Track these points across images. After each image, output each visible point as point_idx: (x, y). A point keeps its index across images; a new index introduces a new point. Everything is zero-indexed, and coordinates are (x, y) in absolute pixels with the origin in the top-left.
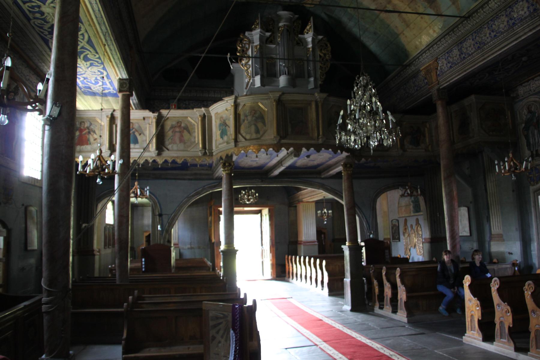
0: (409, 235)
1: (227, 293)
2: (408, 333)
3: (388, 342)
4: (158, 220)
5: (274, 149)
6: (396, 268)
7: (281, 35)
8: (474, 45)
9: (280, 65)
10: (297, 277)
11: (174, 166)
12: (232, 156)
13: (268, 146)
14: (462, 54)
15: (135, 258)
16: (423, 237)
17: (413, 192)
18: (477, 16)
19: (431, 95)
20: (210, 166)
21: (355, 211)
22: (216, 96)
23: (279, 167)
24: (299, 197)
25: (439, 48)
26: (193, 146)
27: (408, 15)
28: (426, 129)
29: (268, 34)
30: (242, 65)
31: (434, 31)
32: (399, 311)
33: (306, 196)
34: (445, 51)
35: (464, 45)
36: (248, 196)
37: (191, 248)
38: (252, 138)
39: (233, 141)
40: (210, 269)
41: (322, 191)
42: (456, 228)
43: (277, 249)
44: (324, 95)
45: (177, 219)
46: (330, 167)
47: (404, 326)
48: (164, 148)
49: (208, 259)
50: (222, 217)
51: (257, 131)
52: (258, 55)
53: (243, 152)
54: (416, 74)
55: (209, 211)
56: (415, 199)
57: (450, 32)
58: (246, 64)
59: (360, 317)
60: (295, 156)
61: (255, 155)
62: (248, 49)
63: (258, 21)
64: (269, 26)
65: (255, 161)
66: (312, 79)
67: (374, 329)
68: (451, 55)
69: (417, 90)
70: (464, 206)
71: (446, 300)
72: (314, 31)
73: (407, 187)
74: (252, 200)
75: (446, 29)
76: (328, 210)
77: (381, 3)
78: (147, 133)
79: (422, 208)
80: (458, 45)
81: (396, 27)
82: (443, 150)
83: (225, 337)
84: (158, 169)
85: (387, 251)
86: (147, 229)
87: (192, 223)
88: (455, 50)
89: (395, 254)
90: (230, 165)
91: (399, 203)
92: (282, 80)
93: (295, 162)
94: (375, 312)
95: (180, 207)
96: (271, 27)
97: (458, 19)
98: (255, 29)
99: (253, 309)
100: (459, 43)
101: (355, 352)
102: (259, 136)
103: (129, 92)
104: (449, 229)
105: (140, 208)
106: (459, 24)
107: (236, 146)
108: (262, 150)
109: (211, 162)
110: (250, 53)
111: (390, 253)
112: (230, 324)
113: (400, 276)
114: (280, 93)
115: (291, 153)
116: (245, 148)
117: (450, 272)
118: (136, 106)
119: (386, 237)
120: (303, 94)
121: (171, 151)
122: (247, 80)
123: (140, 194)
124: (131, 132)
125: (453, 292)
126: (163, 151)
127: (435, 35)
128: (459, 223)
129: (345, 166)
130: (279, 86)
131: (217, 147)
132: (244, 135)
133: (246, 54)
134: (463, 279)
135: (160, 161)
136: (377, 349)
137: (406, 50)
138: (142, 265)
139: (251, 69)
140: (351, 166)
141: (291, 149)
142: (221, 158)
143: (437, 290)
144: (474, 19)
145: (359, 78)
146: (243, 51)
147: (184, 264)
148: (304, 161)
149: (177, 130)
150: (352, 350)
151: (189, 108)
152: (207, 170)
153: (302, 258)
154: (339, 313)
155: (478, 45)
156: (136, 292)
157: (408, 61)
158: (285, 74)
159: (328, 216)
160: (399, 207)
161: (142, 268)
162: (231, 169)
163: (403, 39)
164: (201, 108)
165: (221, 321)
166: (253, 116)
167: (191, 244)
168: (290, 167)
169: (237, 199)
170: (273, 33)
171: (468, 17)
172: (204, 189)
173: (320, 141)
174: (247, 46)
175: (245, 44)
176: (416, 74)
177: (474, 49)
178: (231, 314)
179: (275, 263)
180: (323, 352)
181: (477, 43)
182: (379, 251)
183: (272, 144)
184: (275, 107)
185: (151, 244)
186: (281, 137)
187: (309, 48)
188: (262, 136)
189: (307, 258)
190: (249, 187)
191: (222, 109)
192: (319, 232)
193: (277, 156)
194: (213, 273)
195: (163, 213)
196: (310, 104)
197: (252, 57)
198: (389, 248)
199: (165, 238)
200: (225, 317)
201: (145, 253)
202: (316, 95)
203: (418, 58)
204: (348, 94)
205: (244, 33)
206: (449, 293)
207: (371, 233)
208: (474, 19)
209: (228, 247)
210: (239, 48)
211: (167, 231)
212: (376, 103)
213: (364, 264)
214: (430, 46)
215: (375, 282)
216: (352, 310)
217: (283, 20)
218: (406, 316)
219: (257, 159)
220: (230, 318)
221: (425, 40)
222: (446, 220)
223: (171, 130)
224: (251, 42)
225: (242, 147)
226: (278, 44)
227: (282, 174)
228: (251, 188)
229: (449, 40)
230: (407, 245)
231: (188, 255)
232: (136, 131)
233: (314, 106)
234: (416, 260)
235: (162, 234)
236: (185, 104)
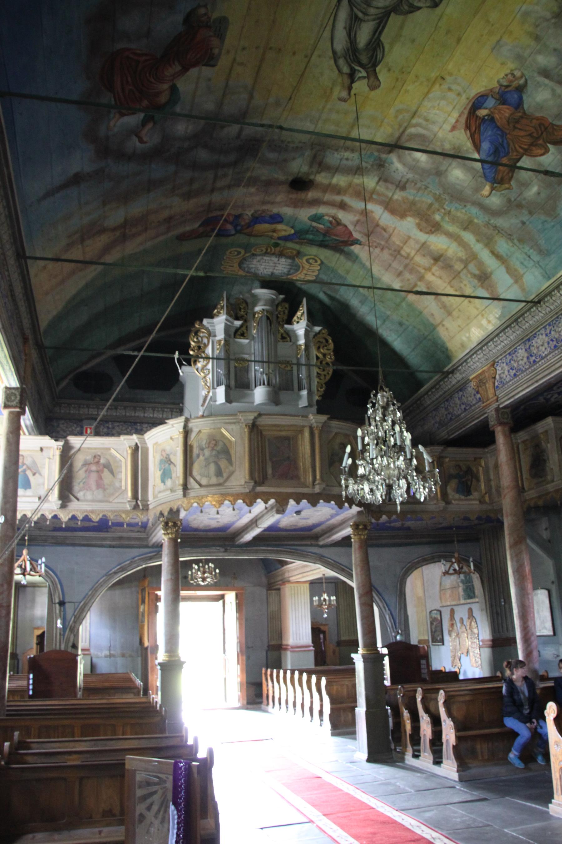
0: (458, 635)
1: (167, 735)
2: (461, 800)
3: (428, 815)
4: (58, 612)
5: (244, 502)
6: (438, 690)
7: (258, 324)
8: (548, 343)
9: (255, 370)
10: (280, 704)
11: (87, 524)
12: (178, 511)
13: (235, 497)
14: (531, 356)
15: (18, 673)
16: (481, 638)
17: (462, 568)
18: (551, 301)
19: (487, 417)
20: (144, 526)
21: (372, 597)
22: (155, 415)
23: (252, 529)
24: (284, 573)
25: (496, 346)
26: (117, 494)
27: (450, 298)
28: (481, 469)
29: (238, 323)
30: (197, 370)
31: (489, 322)
32: (444, 760)
33: (296, 573)
34: (505, 352)
35: (534, 344)
36: (204, 572)
37: (111, 656)
38: (211, 483)
39: (181, 488)
40: (139, 692)
41: (320, 566)
42: (530, 624)
43: (248, 658)
44: (323, 418)
45: (89, 610)
46: (332, 529)
47: (454, 787)
48: (72, 497)
49: (137, 675)
50: (161, 605)
51: (219, 473)
52: (222, 355)
53: (195, 505)
54: (462, 387)
55: (140, 596)
56: (465, 577)
57: (513, 323)
58: (204, 368)
59: (382, 771)
60: (278, 512)
61: (215, 510)
62: (206, 346)
63: (224, 303)
64: (239, 310)
65: (216, 519)
66: (304, 393)
67: (404, 792)
68: (515, 358)
69: (465, 409)
70: (542, 588)
71: (520, 741)
72: (308, 320)
73: (454, 560)
74: (209, 580)
75: (507, 318)
76: (329, 596)
77: (408, 280)
78: (45, 472)
79: (477, 592)
80: (524, 343)
81: (432, 315)
82: (507, 503)
83: (160, 816)
84: (60, 529)
85: (423, 662)
86: (39, 623)
87: (113, 614)
88: (520, 351)
89: (436, 665)
90: (175, 525)
91: (441, 584)
92: (259, 394)
93: (278, 521)
94: (407, 762)
95: (95, 590)
96: (242, 313)
97: (524, 304)
98: (218, 316)
99: (207, 765)
100: (527, 339)
101: (374, 834)
102: (221, 480)
103: (20, 408)
104: (521, 626)
105: (29, 590)
106: (526, 312)
107: (185, 495)
108: (227, 502)
109: (145, 520)
110: (209, 351)
111: (428, 665)
112: (170, 796)
113: (445, 702)
114: (256, 414)
115: (272, 507)
116: (200, 498)
117: (522, 696)
118: (30, 429)
119: (422, 638)
120: (291, 415)
121: (83, 501)
122: (204, 393)
123: (31, 570)
124: (20, 470)
125: (530, 729)
126: (70, 501)
127: (491, 328)
128: (536, 615)
129: (356, 527)
130: (253, 403)
131: (155, 497)
132: (198, 478)
133: (204, 352)
134: (545, 708)
135: (64, 517)
136: (410, 827)
137: (447, 349)
138: (29, 684)
139: (210, 375)
140: (365, 527)
141: (272, 501)
142: (162, 514)
143: (504, 726)
144: (547, 304)
145: (375, 395)
146: (199, 348)
147: (100, 685)
148: (292, 519)
149: (94, 468)
150: (369, 830)
151: (113, 435)
152: (138, 532)
153: (289, 673)
154: (349, 764)
155: (555, 343)
156: (16, 734)
157: (450, 365)
158: (264, 384)
159: (330, 605)
160: (442, 590)
161: (29, 689)
162: (177, 531)
163: (443, 333)
164: (131, 434)
165: (154, 788)
166: (213, 449)
167: (110, 650)
168: (270, 529)
169: (186, 577)
170: (246, 321)
171: (537, 302)
172: (133, 562)
173: (317, 489)
174: (205, 341)
175: (202, 338)
176: (462, 387)
177: (549, 350)
178: (171, 778)
179: (245, 680)
180: (322, 834)
181: (552, 340)
182: (410, 662)
183: (242, 494)
184: (247, 433)
185: (46, 650)
186: (255, 482)
187: (301, 345)
188: (226, 481)
189: (297, 674)
190: (205, 559)
191: (164, 438)
192: (316, 631)
193: (250, 512)
194: (144, 700)
195: (66, 600)
196: (301, 432)
197: (213, 358)
198: (426, 656)
199: (68, 640)
200: (162, 781)
201: (34, 665)
202: (311, 417)
203: (466, 361)
204: (361, 420)
205: (201, 321)
206: (524, 732)
207: (398, 633)
208: (547, 304)
209: (170, 656)
210: (192, 343)
211: (72, 629)
212: (401, 432)
213: (387, 683)
214: (483, 344)
215: (406, 714)
216: (369, 760)
217: (261, 303)
218: (456, 769)
219: (218, 516)
220: (169, 785)
221: (476, 334)
222: (515, 611)
223: (84, 469)
224: (211, 334)
225: (194, 498)
226: (253, 338)
227: (257, 539)
228: (207, 561)
229: (512, 335)
230: (455, 650)
231: (104, 667)
232: (29, 468)
233: (307, 434)
234: (470, 676)
235: (64, 635)
236: (106, 428)
